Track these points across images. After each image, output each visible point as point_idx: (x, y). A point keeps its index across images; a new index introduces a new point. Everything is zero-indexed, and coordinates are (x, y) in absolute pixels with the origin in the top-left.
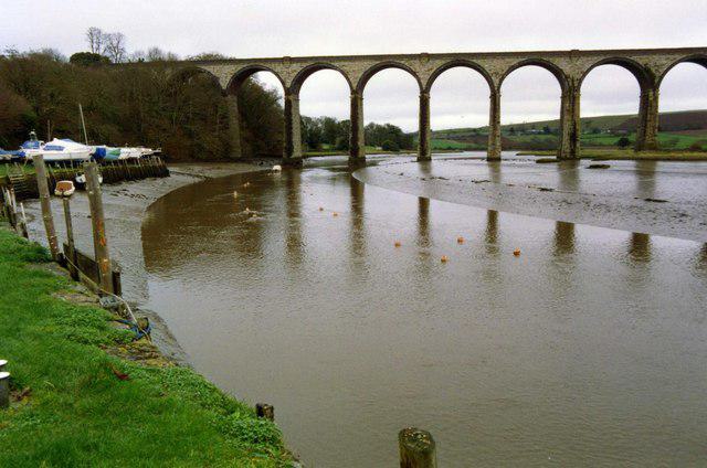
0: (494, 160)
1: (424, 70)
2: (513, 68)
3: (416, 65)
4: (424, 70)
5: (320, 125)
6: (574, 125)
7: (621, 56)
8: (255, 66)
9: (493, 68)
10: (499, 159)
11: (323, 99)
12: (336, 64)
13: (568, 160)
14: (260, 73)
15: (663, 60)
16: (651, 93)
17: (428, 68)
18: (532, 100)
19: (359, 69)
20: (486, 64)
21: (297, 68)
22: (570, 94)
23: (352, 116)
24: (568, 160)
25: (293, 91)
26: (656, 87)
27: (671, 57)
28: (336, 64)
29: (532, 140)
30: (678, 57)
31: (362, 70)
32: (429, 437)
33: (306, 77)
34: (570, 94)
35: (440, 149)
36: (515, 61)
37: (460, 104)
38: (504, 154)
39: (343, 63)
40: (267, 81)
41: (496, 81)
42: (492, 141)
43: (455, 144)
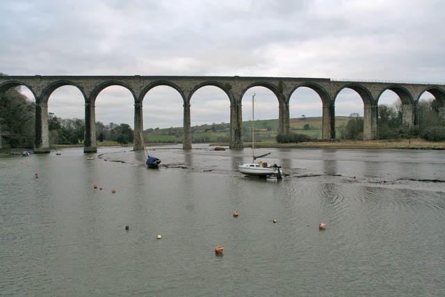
0: (187, 148)
1: (138, 86)
2: (197, 88)
3: (132, 83)
4: (138, 86)
5: (390, 117)
6: (239, 125)
7: (263, 81)
8: (15, 82)
9: (186, 85)
10: (191, 148)
11: (66, 105)
12: (74, 81)
13: (237, 146)
14: (23, 87)
15: (289, 84)
16: (285, 105)
17: (140, 85)
18: (211, 107)
19: (91, 86)
20: (179, 84)
21: (45, 84)
22: (236, 107)
23: (86, 118)
24: (237, 146)
25: (42, 98)
26: (287, 103)
27: (295, 83)
28: (74, 81)
29: (208, 134)
30: (298, 83)
31: (92, 87)
32: (354, 114)
33: (58, 87)
34: (236, 107)
35: (164, 142)
36: (199, 83)
37: (163, 108)
38: (194, 146)
39: (80, 81)
40: (27, 93)
41: (187, 95)
42: (186, 136)
43: (173, 138)
